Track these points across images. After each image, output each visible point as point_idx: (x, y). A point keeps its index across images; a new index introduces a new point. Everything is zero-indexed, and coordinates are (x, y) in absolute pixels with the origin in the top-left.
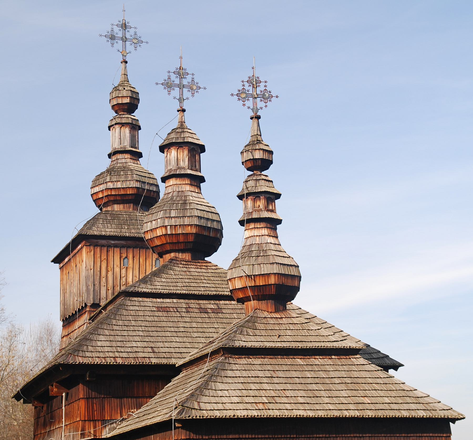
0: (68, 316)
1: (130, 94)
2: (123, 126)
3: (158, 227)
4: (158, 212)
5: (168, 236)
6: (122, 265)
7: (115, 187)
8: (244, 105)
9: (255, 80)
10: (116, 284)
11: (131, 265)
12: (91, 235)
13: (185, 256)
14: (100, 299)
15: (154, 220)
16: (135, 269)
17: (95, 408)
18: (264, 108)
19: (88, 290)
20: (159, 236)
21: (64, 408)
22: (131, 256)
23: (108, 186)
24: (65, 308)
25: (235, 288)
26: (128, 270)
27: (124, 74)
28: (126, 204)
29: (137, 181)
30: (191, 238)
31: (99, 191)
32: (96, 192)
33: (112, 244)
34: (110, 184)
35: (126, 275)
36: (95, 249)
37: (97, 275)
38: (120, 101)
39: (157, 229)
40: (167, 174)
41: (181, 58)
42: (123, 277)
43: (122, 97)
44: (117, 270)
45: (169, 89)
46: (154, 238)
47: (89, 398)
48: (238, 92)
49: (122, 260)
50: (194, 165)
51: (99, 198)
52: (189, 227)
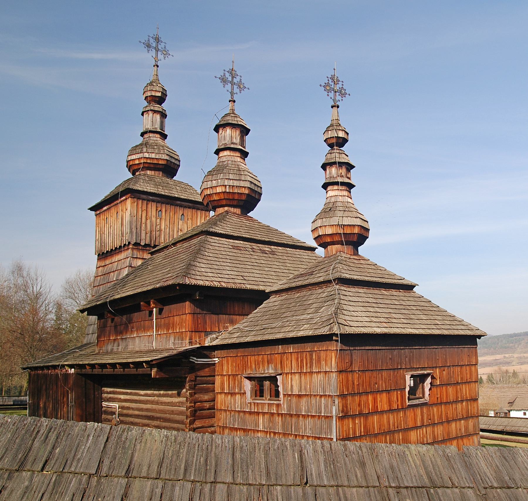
0: (106, 251)
1: (161, 90)
2: (155, 113)
3: (218, 186)
4: (218, 174)
5: (226, 193)
6: (157, 216)
7: (151, 157)
8: (328, 95)
9: (335, 78)
10: (153, 230)
11: (164, 217)
12: (136, 190)
13: (236, 210)
14: (140, 240)
15: (215, 180)
16: (167, 220)
17: (199, 322)
18: (341, 101)
19: (131, 232)
20: (218, 193)
21: (154, 320)
22: (164, 210)
23: (145, 155)
24: (102, 245)
25: (324, 234)
26: (161, 220)
27: (156, 75)
28: (157, 171)
29: (167, 155)
30: (244, 197)
31: (136, 159)
32: (133, 159)
33: (151, 199)
34: (146, 154)
35: (160, 224)
36: (138, 201)
37: (139, 221)
38: (153, 94)
39: (217, 187)
40: (223, 147)
41: (233, 62)
42: (158, 225)
43: (155, 91)
44: (154, 219)
45: (224, 83)
46: (213, 193)
47: (195, 313)
48: (325, 85)
49: (157, 212)
50: (242, 144)
51: (135, 164)
52: (244, 188)
